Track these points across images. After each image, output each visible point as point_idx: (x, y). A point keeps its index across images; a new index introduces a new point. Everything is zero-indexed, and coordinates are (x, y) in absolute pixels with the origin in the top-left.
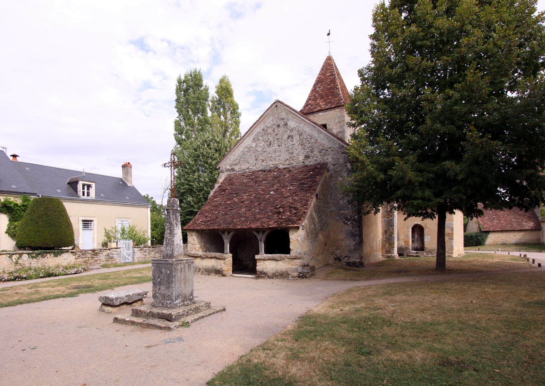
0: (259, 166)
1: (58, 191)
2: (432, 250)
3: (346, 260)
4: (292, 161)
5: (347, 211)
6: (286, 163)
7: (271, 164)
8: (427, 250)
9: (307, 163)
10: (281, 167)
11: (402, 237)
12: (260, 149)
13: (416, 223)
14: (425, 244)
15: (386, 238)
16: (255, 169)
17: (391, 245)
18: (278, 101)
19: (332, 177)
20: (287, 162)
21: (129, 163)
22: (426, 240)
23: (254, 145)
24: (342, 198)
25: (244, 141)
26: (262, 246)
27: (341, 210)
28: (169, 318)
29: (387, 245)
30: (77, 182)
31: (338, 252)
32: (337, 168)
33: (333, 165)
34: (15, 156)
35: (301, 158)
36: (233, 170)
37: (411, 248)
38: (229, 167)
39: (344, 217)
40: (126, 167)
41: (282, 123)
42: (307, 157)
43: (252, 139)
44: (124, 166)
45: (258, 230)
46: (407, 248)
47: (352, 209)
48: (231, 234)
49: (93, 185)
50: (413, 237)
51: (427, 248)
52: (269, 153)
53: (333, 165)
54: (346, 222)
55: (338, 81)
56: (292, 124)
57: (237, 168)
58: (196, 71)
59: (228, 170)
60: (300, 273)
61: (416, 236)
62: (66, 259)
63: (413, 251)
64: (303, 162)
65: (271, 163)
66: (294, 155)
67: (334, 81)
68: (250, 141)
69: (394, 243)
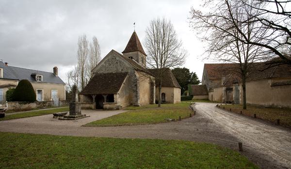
0: (106, 72)
1: (29, 79)
18: (113, 50)
26: (105, 99)
28: (74, 117)
30: (35, 75)
34: (6, 63)
35: (120, 70)
41: (114, 58)
45: (93, 95)
49: (42, 76)
55: (137, 41)
56: (117, 58)
58: (85, 42)
62: (33, 105)
67: (135, 41)
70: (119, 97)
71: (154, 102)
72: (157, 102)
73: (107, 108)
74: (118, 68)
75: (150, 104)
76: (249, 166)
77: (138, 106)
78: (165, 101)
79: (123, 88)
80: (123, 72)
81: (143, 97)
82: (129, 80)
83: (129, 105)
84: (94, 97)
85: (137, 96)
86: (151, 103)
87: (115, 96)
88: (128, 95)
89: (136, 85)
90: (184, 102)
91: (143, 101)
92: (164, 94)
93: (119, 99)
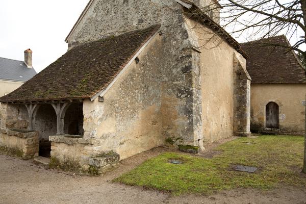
2: (287, 128)
3: (178, 142)
4: (127, 28)
5: (181, 82)
6: (121, 30)
7: (108, 33)
8: (282, 128)
9: (141, 28)
10: (117, 34)
11: (255, 114)
12: (99, 19)
13: (270, 101)
14: (280, 121)
15: (238, 115)
16: (95, 39)
17: (244, 122)
19: (165, 42)
20: (122, 30)
21: (29, 49)
22: (280, 118)
23: (94, 16)
24: (176, 66)
25: (87, 13)
27: (174, 81)
29: (239, 123)
31: (170, 132)
32: (170, 30)
33: (166, 27)
35: (135, 24)
36: (77, 42)
37: (265, 125)
38: (74, 41)
39: (178, 89)
40: (27, 54)
42: (141, 21)
43: (93, 9)
44: (26, 52)
45: (57, 102)
46: (261, 125)
47: (186, 79)
48: (64, 106)
50: (267, 114)
51: (282, 126)
52: (107, 22)
53: (166, 27)
54: (179, 95)
57: (80, 41)
59: (74, 43)
60: (91, 166)
61: (270, 114)
63: (268, 129)
64: (137, 28)
65: (108, 32)
66: (129, 20)
68: (92, 12)
69: (246, 120)
70: (106, 116)
71: (248, 130)
72: (255, 129)
73: (61, 158)
74: (130, 17)
75: (235, 134)
76: (191, 112)
77: (192, 150)
78: (277, 126)
79: (131, 76)
80: (145, 26)
81: (212, 119)
82: (161, 51)
83: (160, 142)
84: (59, 111)
85: (189, 112)
86: (238, 132)
87: (87, 109)
88: (155, 107)
89: (187, 70)
90: (236, 138)
91: (213, 128)
92: (273, 108)
93: (10, 140)
